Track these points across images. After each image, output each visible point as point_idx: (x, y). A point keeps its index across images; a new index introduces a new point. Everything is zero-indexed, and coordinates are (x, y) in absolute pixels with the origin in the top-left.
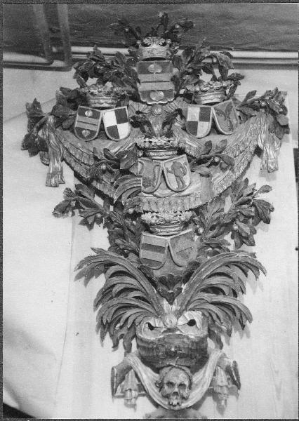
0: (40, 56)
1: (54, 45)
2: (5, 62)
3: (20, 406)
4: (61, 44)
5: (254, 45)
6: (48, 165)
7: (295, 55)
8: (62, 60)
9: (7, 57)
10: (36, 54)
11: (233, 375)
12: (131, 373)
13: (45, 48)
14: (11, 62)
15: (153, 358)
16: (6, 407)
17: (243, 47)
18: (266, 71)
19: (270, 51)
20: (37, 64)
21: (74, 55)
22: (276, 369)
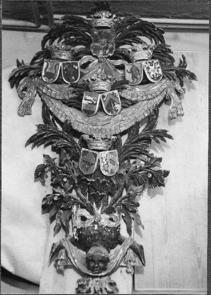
0: (31, 22)
1: (41, 14)
2: (208, 32)
3: (15, 271)
4: (46, 12)
5: (186, 14)
6: (22, 99)
7: (207, 22)
8: (47, 24)
9: (5, 22)
10: (29, 20)
11: (139, 252)
12: (63, 251)
13: (35, 15)
14: (9, 26)
15: (83, 241)
16: (4, 270)
17: (176, 16)
18: (192, 34)
19: (169, 18)
20: (27, 27)
21: (55, 21)
22: (198, 246)
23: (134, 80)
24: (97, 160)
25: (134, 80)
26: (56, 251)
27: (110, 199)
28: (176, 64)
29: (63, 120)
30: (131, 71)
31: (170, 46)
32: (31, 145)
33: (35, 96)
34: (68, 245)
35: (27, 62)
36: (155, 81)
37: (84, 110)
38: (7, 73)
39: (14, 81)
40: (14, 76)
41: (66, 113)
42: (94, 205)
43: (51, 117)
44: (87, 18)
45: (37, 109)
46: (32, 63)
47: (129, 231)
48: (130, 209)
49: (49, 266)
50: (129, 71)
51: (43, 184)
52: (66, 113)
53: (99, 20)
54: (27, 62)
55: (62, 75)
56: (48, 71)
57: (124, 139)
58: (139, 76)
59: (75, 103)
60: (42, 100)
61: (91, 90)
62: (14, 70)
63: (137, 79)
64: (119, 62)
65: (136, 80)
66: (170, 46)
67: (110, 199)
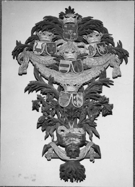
11: (96, 149)
23: (90, 54)
24: (70, 98)
25: (90, 54)
26: (46, 149)
27: (78, 120)
28: (116, 45)
29: (48, 76)
30: (89, 49)
31: (112, 35)
32: (28, 92)
33: (29, 62)
34: (54, 146)
35: (23, 42)
36: (103, 55)
37: (60, 70)
38: (9, 47)
39: (15, 53)
40: (17, 50)
41: (47, 72)
42: (74, 180)
43: (39, 74)
44: (71, 158)
45: (30, 70)
46: (27, 43)
47: (91, 139)
48: (91, 127)
49: (42, 156)
50: (87, 48)
51: (38, 111)
52: (47, 72)
53: (68, 19)
54: (23, 42)
55: (46, 48)
56: (37, 47)
57: (85, 87)
58: (93, 52)
59: (55, 67)
60: (33, 65)
61: (65, 58)
62: (92, 93)
63: (93, 53)
64: (81, 44)
65: (92, 53)
66: (112, 35)
67: (78, 120)
